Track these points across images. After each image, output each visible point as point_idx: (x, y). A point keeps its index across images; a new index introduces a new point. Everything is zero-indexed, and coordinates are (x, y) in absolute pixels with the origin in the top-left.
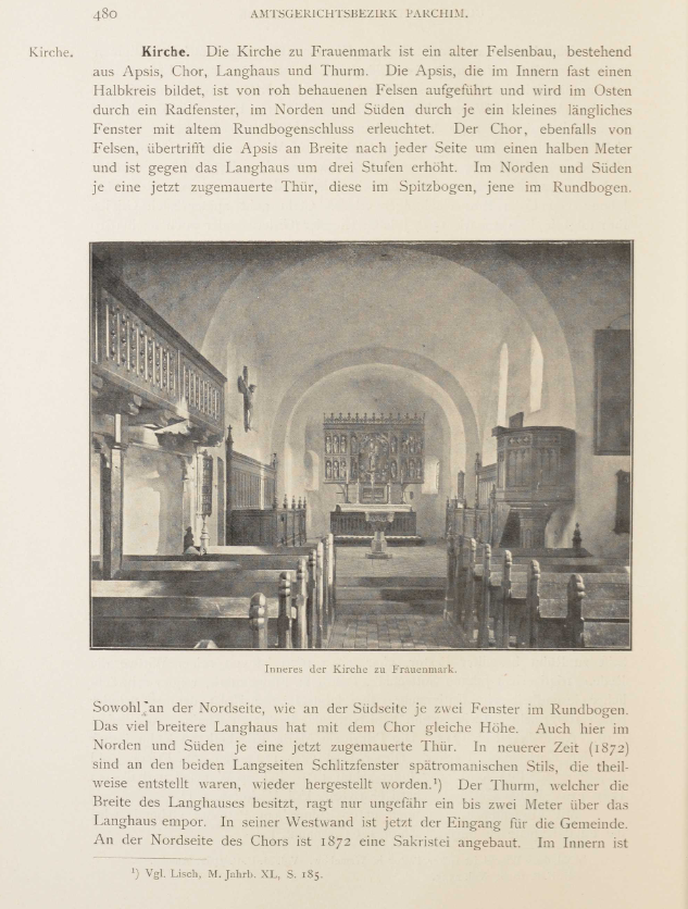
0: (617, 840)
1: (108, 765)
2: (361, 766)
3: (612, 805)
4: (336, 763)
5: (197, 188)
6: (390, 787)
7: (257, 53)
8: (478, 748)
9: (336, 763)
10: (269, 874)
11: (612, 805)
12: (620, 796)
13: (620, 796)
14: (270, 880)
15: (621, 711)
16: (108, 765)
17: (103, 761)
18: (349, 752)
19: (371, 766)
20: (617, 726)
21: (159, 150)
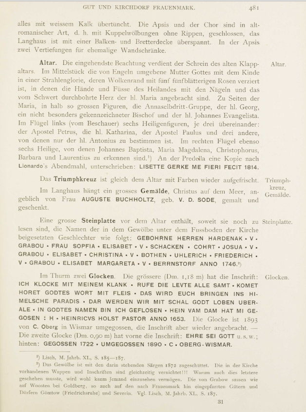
0: (20, 87)
1: (43, 229)
2: (113, 116)
3: (253, 99)
4: (76, 237)
5: (255, 222)
6: (131, 34)
7: (248, 231)
8: (183, 142)
9: (22, 342)
10: (192, 393)
11: (253, 99)
12: (255, 95)
13: (255, 95)
14: (193, 396)
15: (21, 344)
16: (43, 229)
17: (138, 157)
18: (150, 36)
19: (118, 116)
20: (105, 228)
21: (224, 125)
